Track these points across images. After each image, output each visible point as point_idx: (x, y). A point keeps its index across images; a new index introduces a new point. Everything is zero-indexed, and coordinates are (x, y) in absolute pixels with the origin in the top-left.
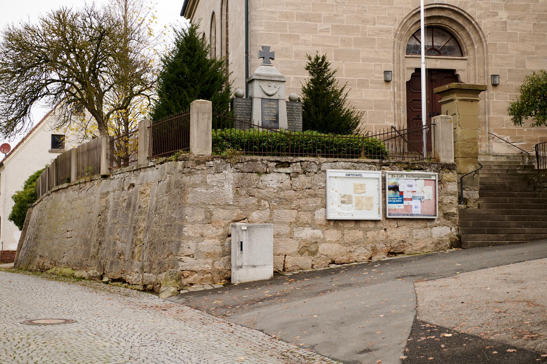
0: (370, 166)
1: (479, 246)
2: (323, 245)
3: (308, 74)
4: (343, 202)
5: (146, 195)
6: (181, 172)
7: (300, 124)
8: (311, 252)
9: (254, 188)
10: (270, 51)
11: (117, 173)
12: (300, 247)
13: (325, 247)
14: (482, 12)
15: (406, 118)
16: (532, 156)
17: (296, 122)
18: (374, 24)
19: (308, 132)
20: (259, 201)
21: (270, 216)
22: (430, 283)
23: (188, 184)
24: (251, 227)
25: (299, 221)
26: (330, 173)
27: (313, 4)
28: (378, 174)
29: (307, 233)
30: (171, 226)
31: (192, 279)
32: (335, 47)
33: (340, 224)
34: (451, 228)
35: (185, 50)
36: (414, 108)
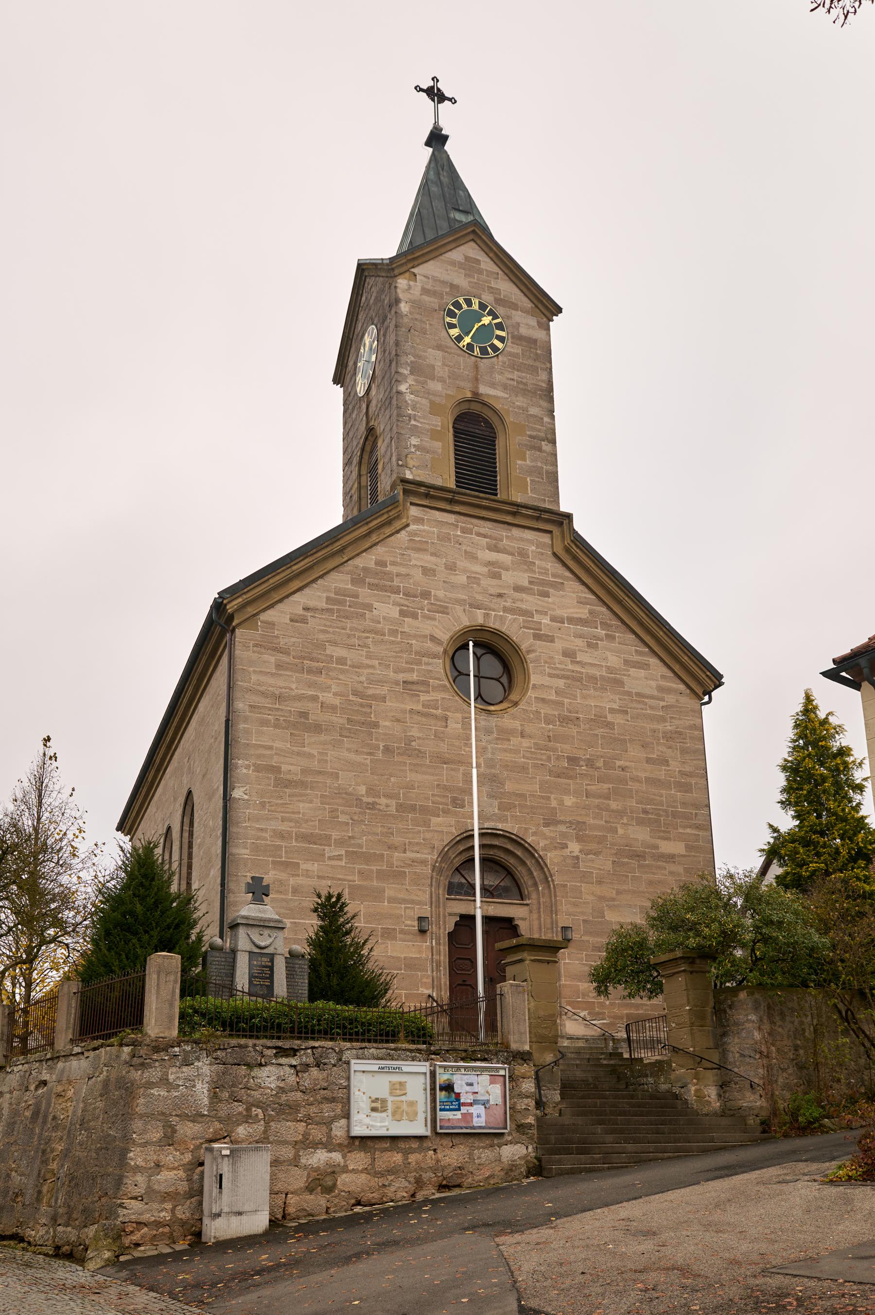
0: (413, 1054)
1: (567, 1174)
2: (344, 1175)
3: (316, 918)
4: (374, 1109)
5: (66, 1098)
6: (127, 1063)
7: (305, 990)
8: (326, 1188)
9: (241, 1089)
10: (264, 884)
11: (19, 1063)
13: (347, 1180)
14: (547, 842)
15: (448, 983)
16: (617, 1039)
18: (405, 852)
19: (320, 1004)
20: (248, 1110)
21: (265, 1132)
22: (518, 1237)
23: (138, 1083)
24: (237, 1150)
25: (308, 1139)
26: (356, 1065)
27: (319, 820)
28: (424, 1067)
29: (320, 1158)
30: (107, 1149)
31: (138, 1236)
32: (350, 881)
33: (370, 1143)
34: (527, 1147)
35: (137, 878)
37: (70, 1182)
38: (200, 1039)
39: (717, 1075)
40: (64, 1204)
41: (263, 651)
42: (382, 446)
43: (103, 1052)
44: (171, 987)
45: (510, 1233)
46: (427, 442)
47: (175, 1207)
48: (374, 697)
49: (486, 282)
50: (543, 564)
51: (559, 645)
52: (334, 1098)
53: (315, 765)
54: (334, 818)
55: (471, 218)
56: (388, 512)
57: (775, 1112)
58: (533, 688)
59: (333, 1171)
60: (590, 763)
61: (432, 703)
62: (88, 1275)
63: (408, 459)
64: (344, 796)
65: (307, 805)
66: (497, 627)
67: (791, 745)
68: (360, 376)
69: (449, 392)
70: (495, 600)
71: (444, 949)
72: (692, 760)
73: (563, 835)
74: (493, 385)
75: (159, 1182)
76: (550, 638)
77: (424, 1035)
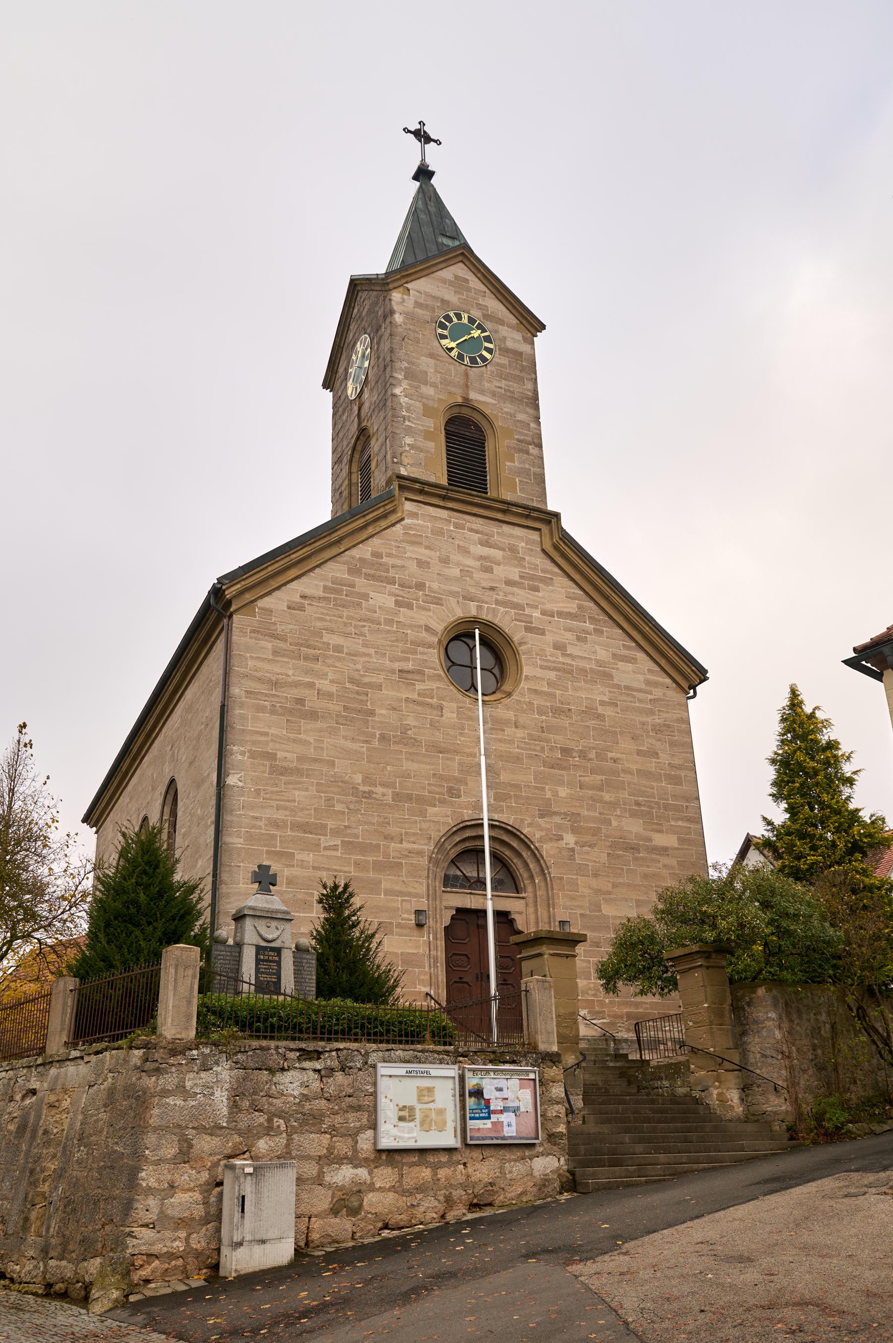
1: (604, 1189)
2: (371, 1195)
4: (401, 1119)
5: (61, 1109)
7: (312, 987)
9: (263, 1097)
12: (334, 1202)
13: (374, 1199)
14: (543, 833)
15: (445, 980)
16: (618, 1040)
17: (306, 984)
18: (401, 842)
19: (337, 1001)
20: (270, 1120)
21: (287, 1146)
23: (152, 1091)
25: (332, 1153)
26: (384, 1069)
27: (315, 808)
28: (452, 1071)
29: (344, 1175)
31: (149, 1270)
32: (345, 872)
33: (397, 1157)
36: (454, 966)
37: (65, 1207)
38: (219, 1041)
39: (738, 1077)
40: (58, 1233)
41: (260, 636)
42: (375, 445)
43: (108, 1056)
44: (189, 982)
45: (581, 1261)
46: (421, 441)
47: (189, 1235)
48: (370, 685)
49: (474, 299)
50: (533, 560)
51: (549, 638)
52: (360, 1106)
53: (311, 752)
54: (329, 806)
55: (457, 243)
56: (384, 506)
57: (800, 1116)
58: (525, 679)
59: (359, 1190)
60: (583, 754)
61: (427, 692)
62: (95, 1319)
63: (403, 457)
64: (340, 784)
65: (303, 793)
66: (490, 619)
67: (778, 738)
68: (351, 380)
69: (440, 397)
70: (488, 593)
71: (441, 945)
72: (680, 752)
73: (559, 827)
74: (482, 392)
75: (173, 1206)
76: (540, 631)
77: (445, 1036)
